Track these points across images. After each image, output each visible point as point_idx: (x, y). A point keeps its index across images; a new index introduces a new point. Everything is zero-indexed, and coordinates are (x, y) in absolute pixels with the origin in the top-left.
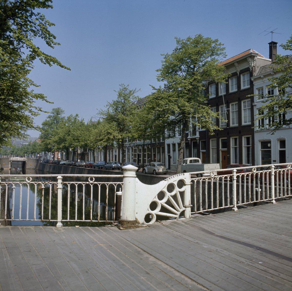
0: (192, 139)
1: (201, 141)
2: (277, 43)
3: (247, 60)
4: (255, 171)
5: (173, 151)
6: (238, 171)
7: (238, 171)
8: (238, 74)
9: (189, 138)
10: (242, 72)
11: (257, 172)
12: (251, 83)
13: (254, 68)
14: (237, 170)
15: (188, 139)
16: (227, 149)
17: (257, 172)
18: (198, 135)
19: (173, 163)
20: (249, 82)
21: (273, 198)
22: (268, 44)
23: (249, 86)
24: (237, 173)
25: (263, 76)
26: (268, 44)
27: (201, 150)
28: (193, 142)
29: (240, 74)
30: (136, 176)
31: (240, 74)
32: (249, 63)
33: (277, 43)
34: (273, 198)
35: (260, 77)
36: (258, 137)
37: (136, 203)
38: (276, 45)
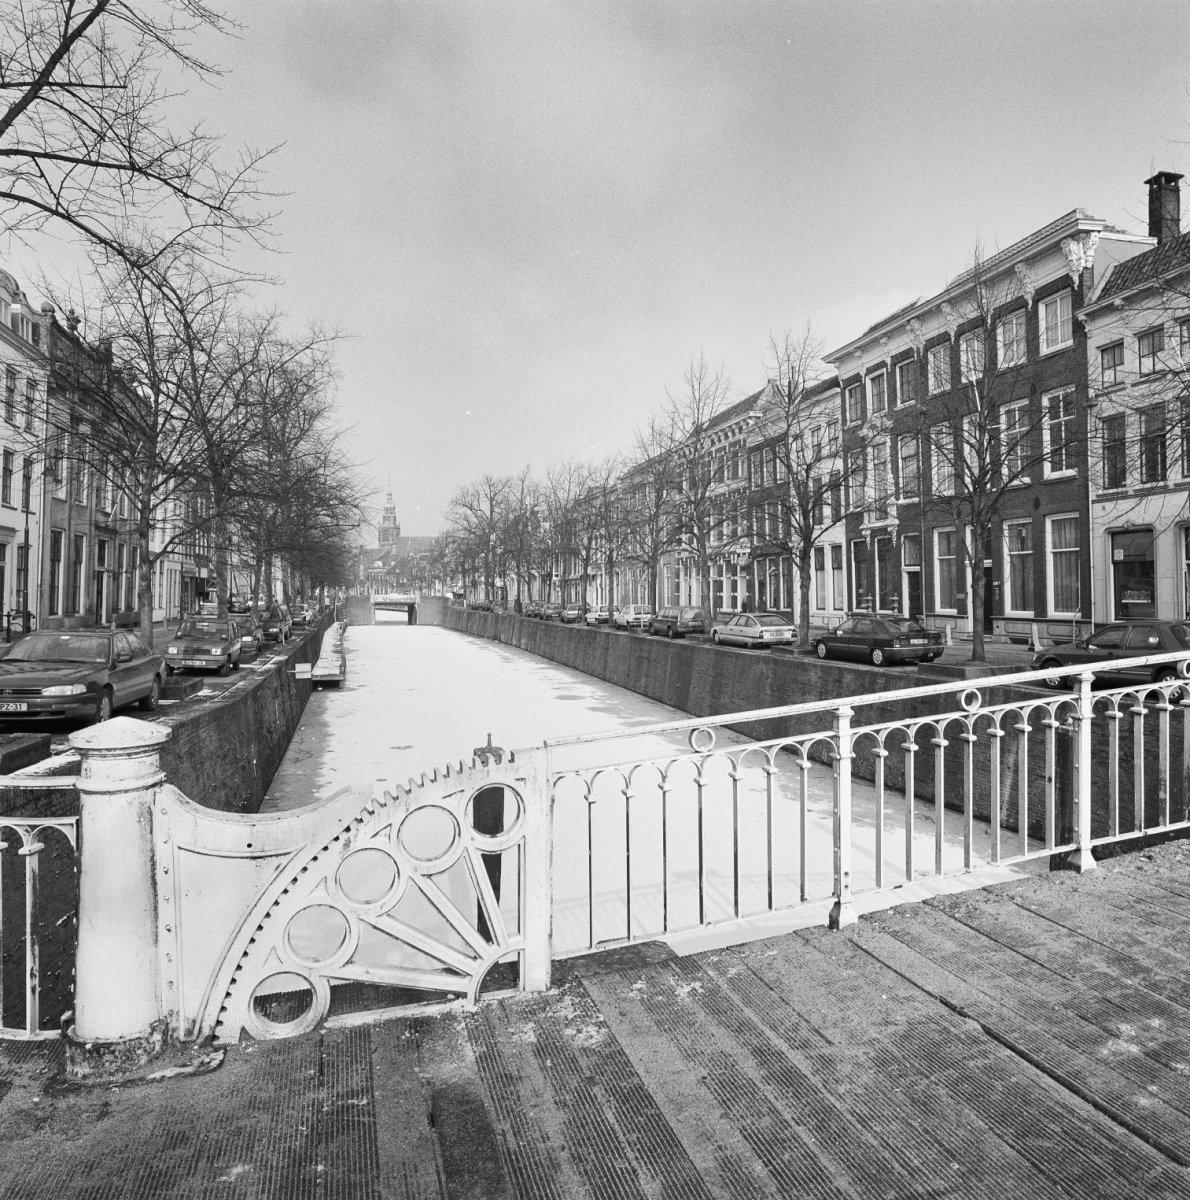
0: (875, 532)
1: (940, 534)
2: (1181, 176)
3: (1061, 248)
4: (976, 709)
5: (834, 569)
6: (861, 716)
7: (861, 716)
8: (1030, 302)
9: (866, 529)
10: (1043, 293)
11: (986, 711)
12: (1079, 330)
13: (1087, 275)
14: (858, 709)
15: (862, 530)
16: (990, 561)
17: (986, 711)
18: (892, 521)
19: (835, 609)
20: (1069, 327)
21: (1086, 842)
22: (1146, 182)
23: (1070, 343)
24: (855, 722)
25: (1123, 299)
26: (1146, 182)
27: (903, 567)
28: (879, 541)
29: (1036, 302)
30: (162, 776)
31: (1036, 302)
32: (1070, 258)
33: (1181, 176)
34: (1086, 842)
35: (1112, 304)
36: (1104, 516)
37: (173, 929)
38: (1176, 183)
